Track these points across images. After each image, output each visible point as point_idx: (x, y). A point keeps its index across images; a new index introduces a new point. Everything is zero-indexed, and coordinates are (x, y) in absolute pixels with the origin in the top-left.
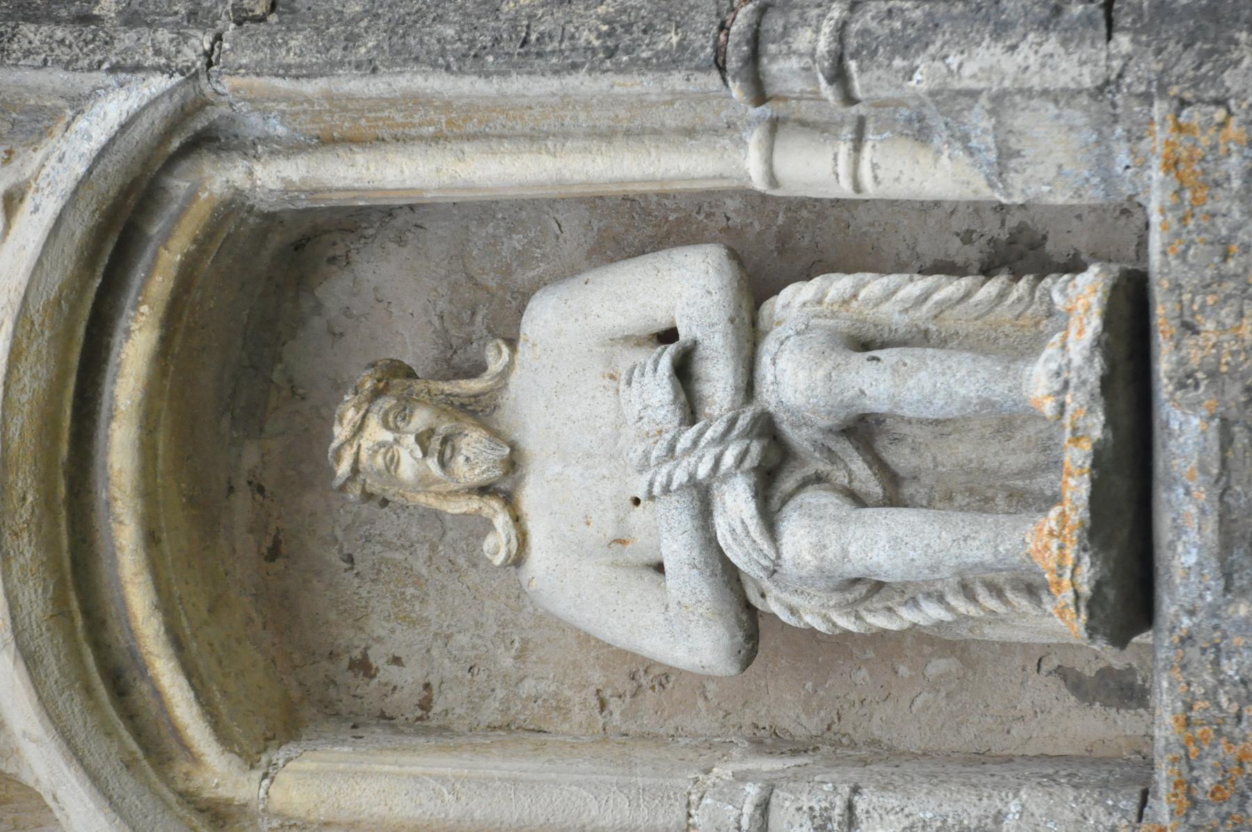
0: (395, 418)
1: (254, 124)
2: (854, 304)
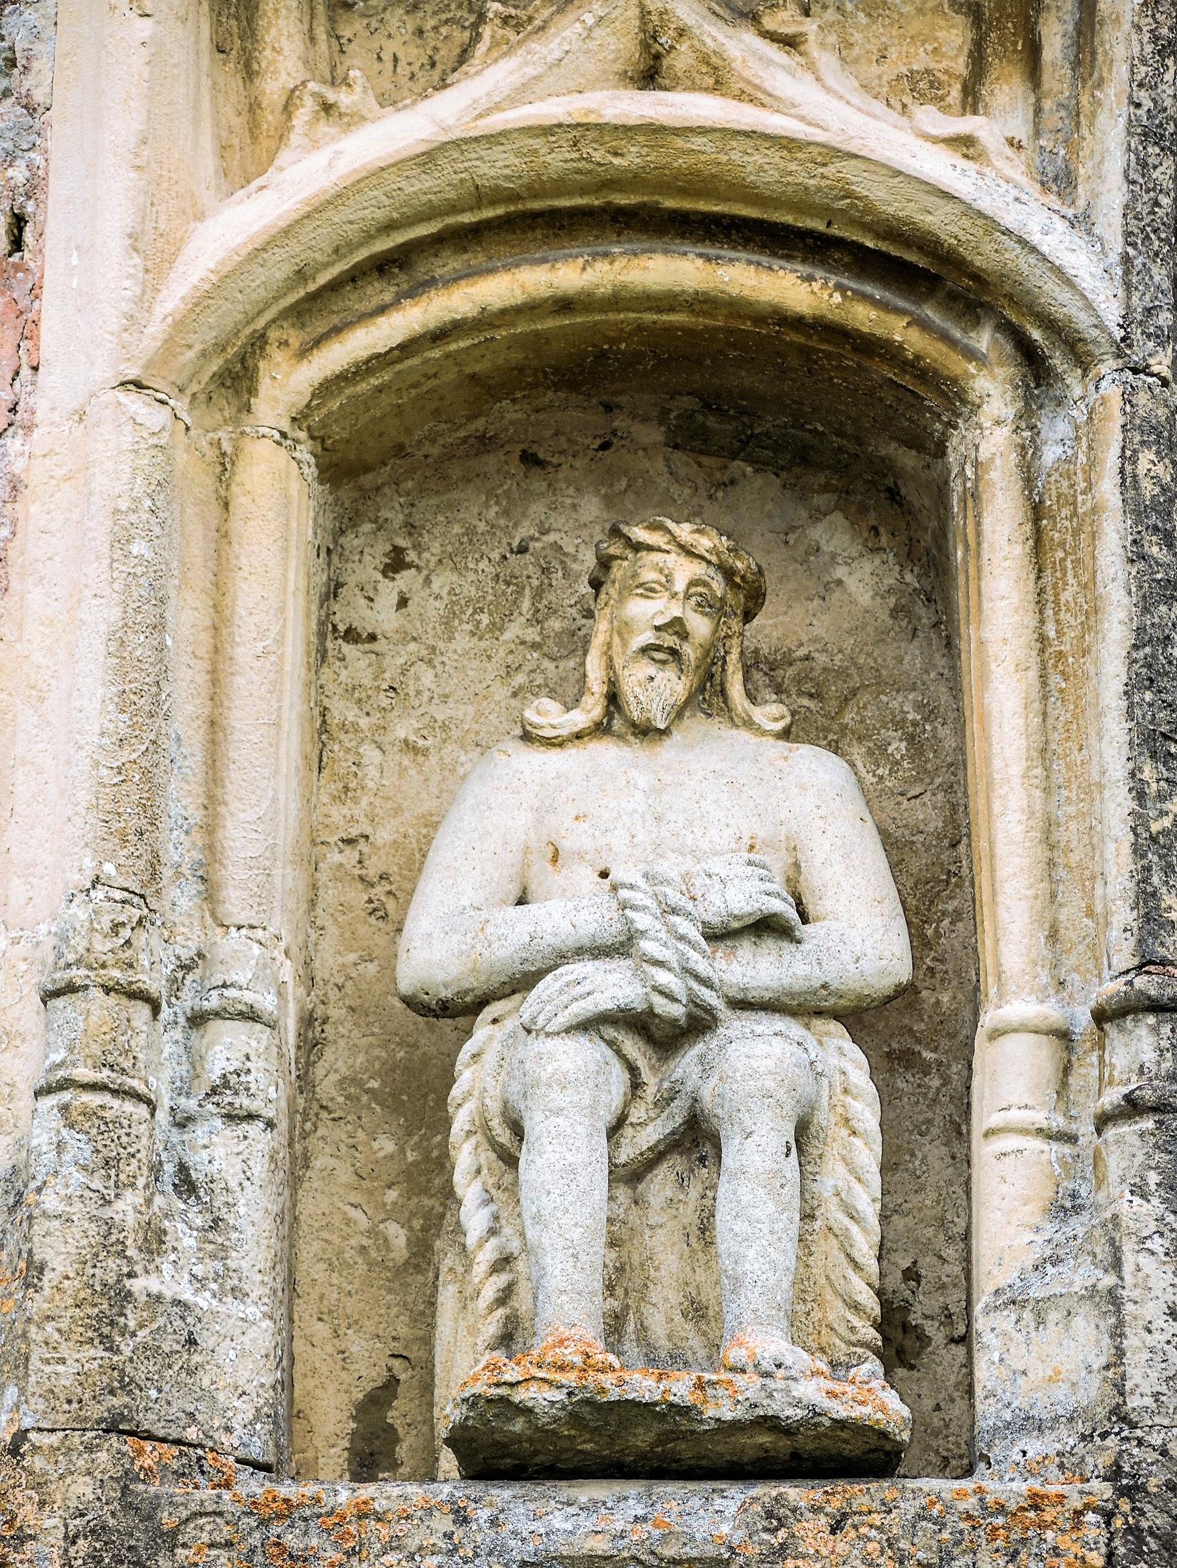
0: (701, 595)
1: (1056, 431)
2: (845, 1132)
